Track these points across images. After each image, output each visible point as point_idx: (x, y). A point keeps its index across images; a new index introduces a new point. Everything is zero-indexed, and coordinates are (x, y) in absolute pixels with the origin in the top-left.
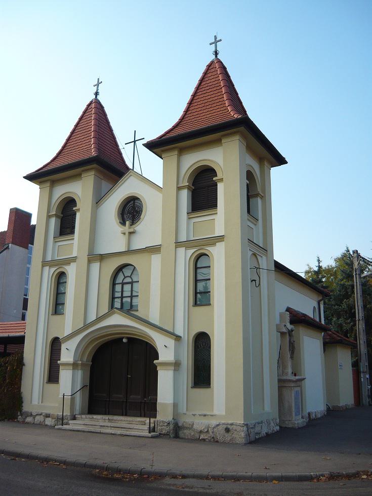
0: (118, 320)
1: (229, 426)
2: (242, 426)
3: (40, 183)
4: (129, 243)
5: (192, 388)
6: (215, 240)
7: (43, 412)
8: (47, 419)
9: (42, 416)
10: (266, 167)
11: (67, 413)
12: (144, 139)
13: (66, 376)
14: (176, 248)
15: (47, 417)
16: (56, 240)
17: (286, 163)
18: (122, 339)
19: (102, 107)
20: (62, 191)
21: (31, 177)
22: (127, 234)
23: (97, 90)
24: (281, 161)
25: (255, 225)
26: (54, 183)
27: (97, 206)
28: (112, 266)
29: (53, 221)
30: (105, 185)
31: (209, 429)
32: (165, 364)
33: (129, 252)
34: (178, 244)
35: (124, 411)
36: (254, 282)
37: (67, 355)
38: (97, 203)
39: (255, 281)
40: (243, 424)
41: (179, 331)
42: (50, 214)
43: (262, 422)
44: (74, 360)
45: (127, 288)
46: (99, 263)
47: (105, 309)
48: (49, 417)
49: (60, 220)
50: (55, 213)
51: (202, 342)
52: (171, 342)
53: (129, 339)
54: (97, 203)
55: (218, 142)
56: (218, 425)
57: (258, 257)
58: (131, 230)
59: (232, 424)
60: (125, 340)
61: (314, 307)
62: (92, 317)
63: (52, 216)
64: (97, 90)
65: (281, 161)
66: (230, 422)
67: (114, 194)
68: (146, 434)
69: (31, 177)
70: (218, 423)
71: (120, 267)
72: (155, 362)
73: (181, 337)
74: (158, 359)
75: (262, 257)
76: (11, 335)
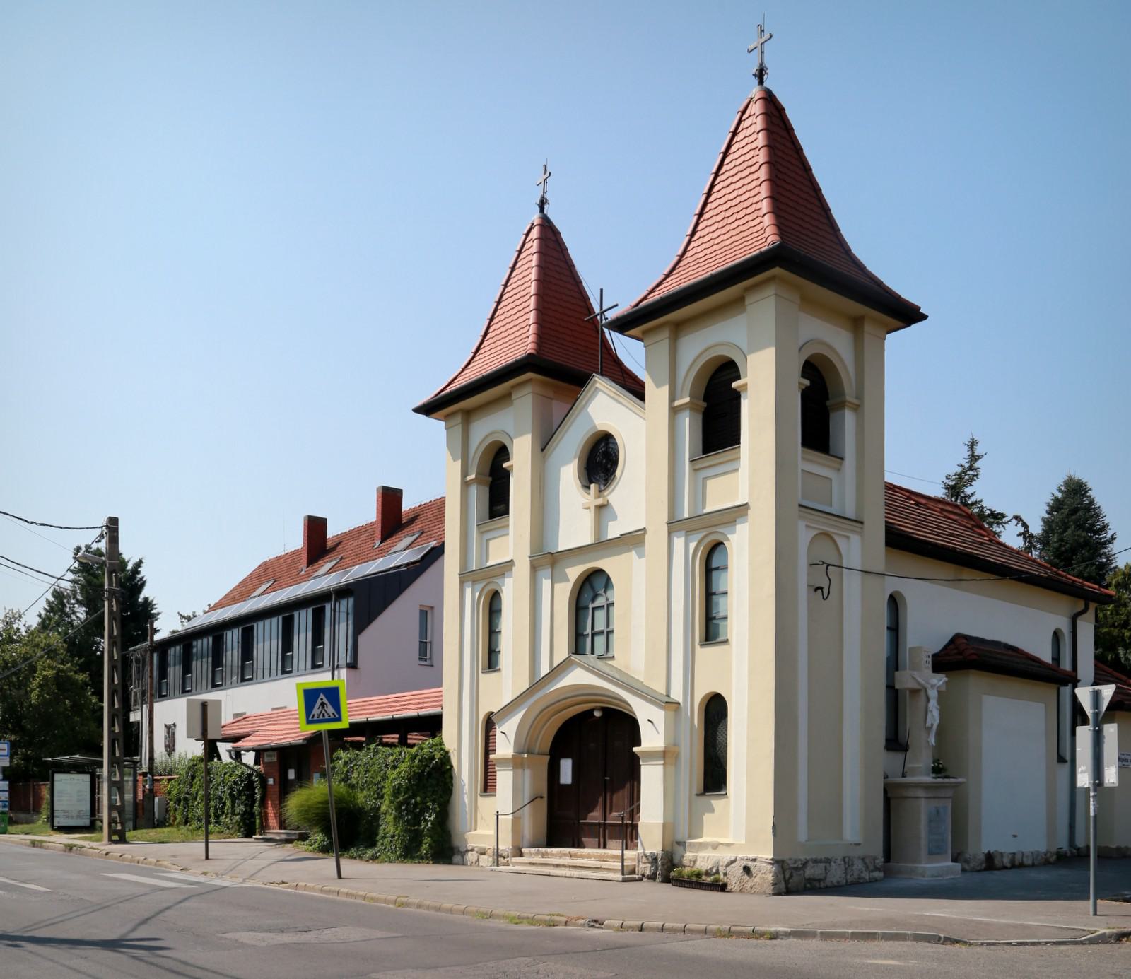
0: (578, 677)
1: (750, 864)
2: (770, 863)
3: (446, 418)
4: (599, 526)
5: (697, 795)
6: (739, 512)
7: (475, 845)
8: (483, 856)
9: (474, 853)
10: (867, 338)
11: (506, 845)
12: (617, 305)
13: (504, 779)
14: (670, 533)
15: (482, 854)
16: (697, 467)
17: (924, 317)
18: (590, 712)
19: (556, 233)
20: (485, 429)
21: (427, 409)
22: (593, 509)
23: (545, 192)
24: (907, 314)
25: (839, 470)
26: (678, 329)
27: (544, 457)
28: (574, 572)
29: (474, 491)
30: (558, 408)
31: (720, 868)
32: (652, 755)
33: (602, 545)
34: (674, 525)
35: (602, 840)
36: (819, 591)
37: (504, 747)
38: (543, 450)
39: (821, 588)
40: (771, 860)
41: (677, 694)
42: (677, 403)
43: (828, 861)
44: (665, 743)
45: (601, 616)
46: (550, 570)
47: (562, 652)
48: (484, 854)
49: (487, 490)
50: (687, 400)
51: (715, 709)
52: (659, 715)
53: (603, 709)
54: (543, 450)
55: (738, 303)
56: (733, 862)
57: (836, 538)
58: (600, 501)
59: (754, 860)
60: (597, 714)
61: (245, 713)
62: (544, 669)
63: (682, 407)
64: (545, 192)
65: (907, 314)
66: (752, 856)
67: (571, 428)
68: (619, 876)
69: (427, 409)
70: (733, 858)
71: (585, 577)
72: (635, 749)
73: (679, 703)
74: (639, 744)
75: (848, 537)
76: (423, 712)
